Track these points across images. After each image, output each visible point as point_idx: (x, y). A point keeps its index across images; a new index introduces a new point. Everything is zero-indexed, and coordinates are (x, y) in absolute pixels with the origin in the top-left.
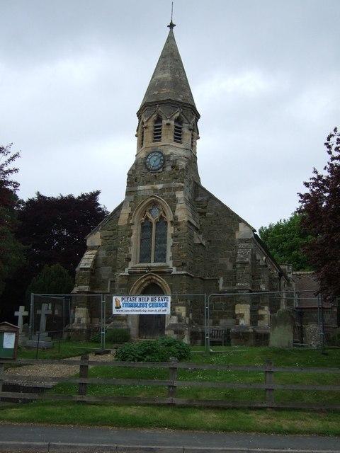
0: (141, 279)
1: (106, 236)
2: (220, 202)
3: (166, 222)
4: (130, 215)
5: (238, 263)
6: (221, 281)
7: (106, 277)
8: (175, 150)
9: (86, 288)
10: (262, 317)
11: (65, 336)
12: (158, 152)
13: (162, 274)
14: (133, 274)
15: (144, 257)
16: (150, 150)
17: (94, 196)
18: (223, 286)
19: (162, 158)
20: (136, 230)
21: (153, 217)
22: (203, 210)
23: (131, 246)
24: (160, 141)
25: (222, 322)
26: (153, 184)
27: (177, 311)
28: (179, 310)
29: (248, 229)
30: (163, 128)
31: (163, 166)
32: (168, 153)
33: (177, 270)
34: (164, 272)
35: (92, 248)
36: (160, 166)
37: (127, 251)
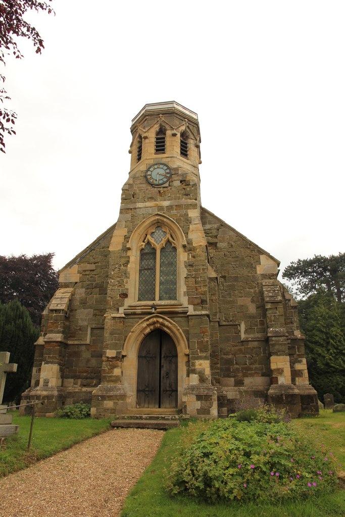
1: (85, 271)
3: (175, 249)
4: (127, 238)
5: (267, 302)
6: (243, 327)
7: (86, 323)
9: (58, 337)
11: (24, 404)
13: (172, 314)
14: (131, 315)
15: (146, 292)
16: (152, 162)
18: (246, 332)
19: (168, 171)
20: (134, 257)
21: (158, 241)
22: (215, 240)
24: (164, 153)
25: (248, 381)
27: (197, 367)
28: (200, 365)
29: (271, 262)
31: (170, 179)
32: (175, 166)
33: (195, 310)
34: (177, 313)
35: (66, 285)
36: (165, 180)
37: (121, 284)
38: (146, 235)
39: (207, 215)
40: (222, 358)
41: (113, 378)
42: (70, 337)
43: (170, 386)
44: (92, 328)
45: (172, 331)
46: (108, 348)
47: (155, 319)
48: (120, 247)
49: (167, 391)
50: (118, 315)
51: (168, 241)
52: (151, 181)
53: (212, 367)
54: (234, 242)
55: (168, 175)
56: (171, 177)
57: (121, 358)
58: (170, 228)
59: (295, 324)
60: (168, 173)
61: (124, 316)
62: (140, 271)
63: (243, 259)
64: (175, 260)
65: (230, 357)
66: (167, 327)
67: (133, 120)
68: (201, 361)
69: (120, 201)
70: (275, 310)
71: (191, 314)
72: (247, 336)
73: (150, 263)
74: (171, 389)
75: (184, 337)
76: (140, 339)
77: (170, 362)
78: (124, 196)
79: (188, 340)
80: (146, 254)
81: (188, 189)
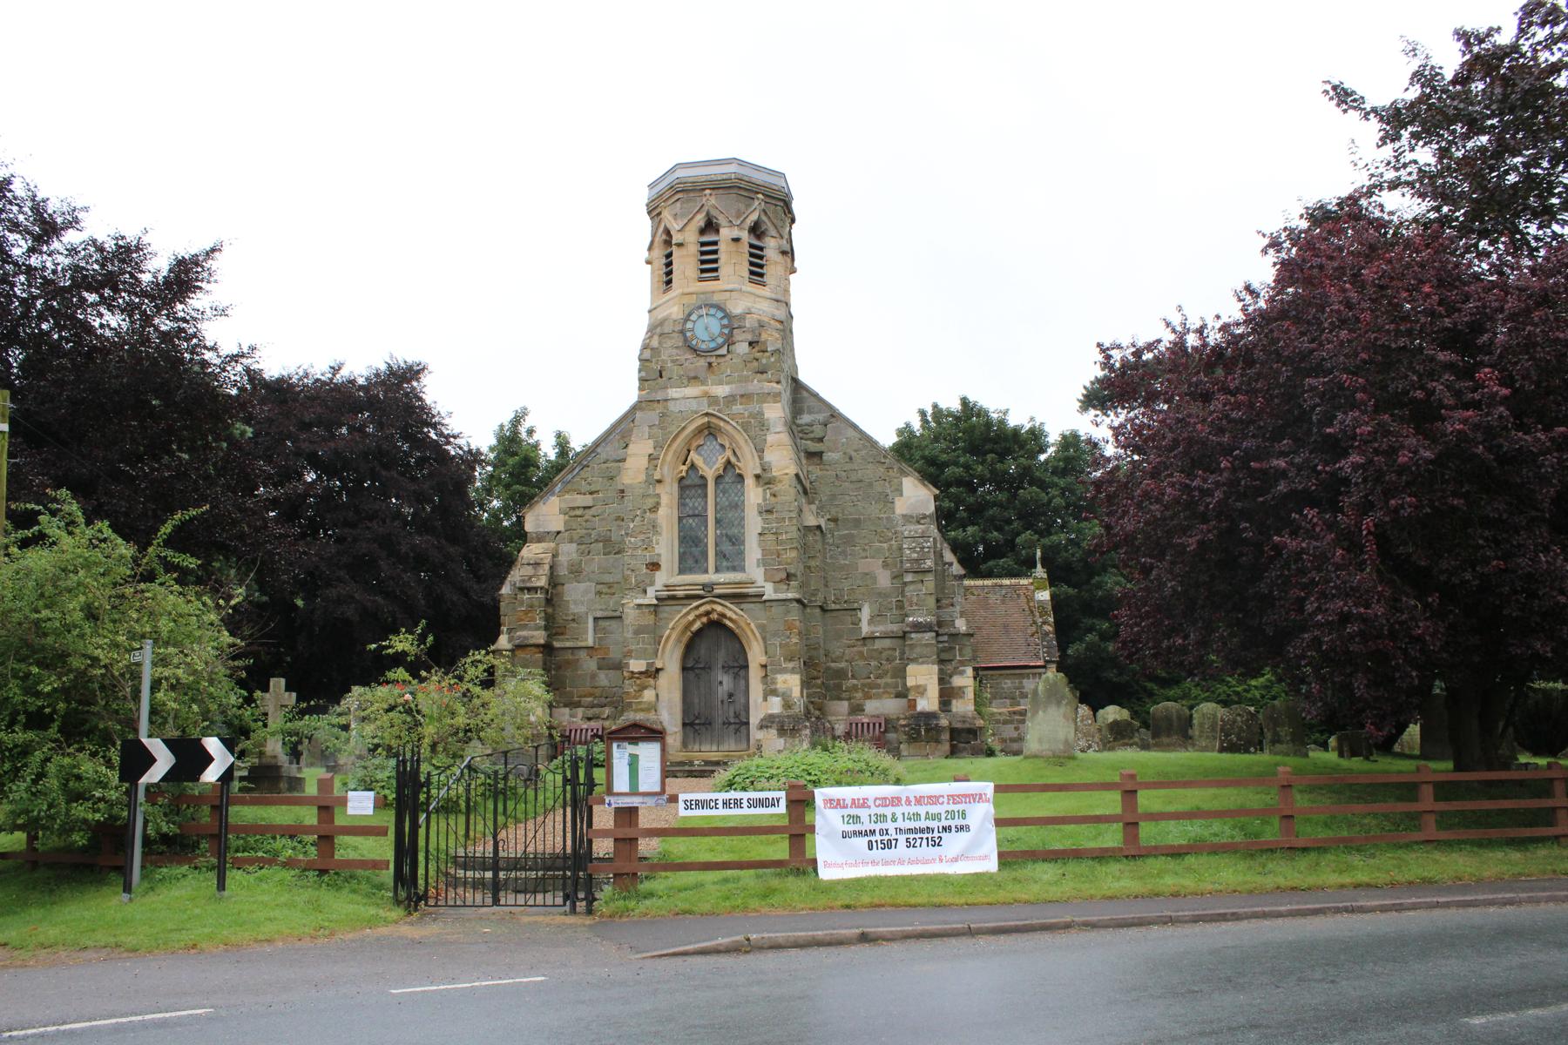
0: (688, 613)
2: (855, 427)
3: (741, 478)
4: (652, 458)
6: (865, 614)
8: (749, 302)
10: (959, 692)
12: (712, 306)
14: (669, 599)
15: (691, 552)
16: (693, 300)
17: (412, 373)
18: (871, 622)
19: (725, 322)
20: (668, 496)
22: (814, 447)
23: (657, 533)
24: (717, 279)
26: (703, 383)
27: (780, 686)
30: (722, 247)
33: (776, 591)
35: (540, 538)
36: (720, 340)
37: (648, 546)
38: (689, 451)
39: (805, 394)
40: (828, 668)
41: (642, 706)
42: (556, 634)
43: (737, 716)
44: (596, 619)
45: (739, 627)
46: (631, 657)
47: (707, 607)
48: (642, 477)
49: (730, 724)
50: (646, 602)
51: (729, 462)
52: (694, 342)
53: (806, 684)
54: (856, 451)
55: (726, 331)
56: (731, 334)
57: (654, 673)
58: (731, 438)
59: (958, 607)
60: (724, 326)
61: (655, 602)
62: (680, 519)
63: (870, 485)
64: (742, 498)
65: (843, 665)
66: (731, 619)
67: (651, 186)
68: (787, 677)
69: (636, 384)
70: (920, 586)
71: (770, 598)
72: (873, 628)
73: (696, 504)
74: (737, 721)
75: (758, 634)
76: (685, 639)
77: (736, 676)
78: (643, 374)
79: (765, 642)
80: (688, 487)
81: (764, 361)
